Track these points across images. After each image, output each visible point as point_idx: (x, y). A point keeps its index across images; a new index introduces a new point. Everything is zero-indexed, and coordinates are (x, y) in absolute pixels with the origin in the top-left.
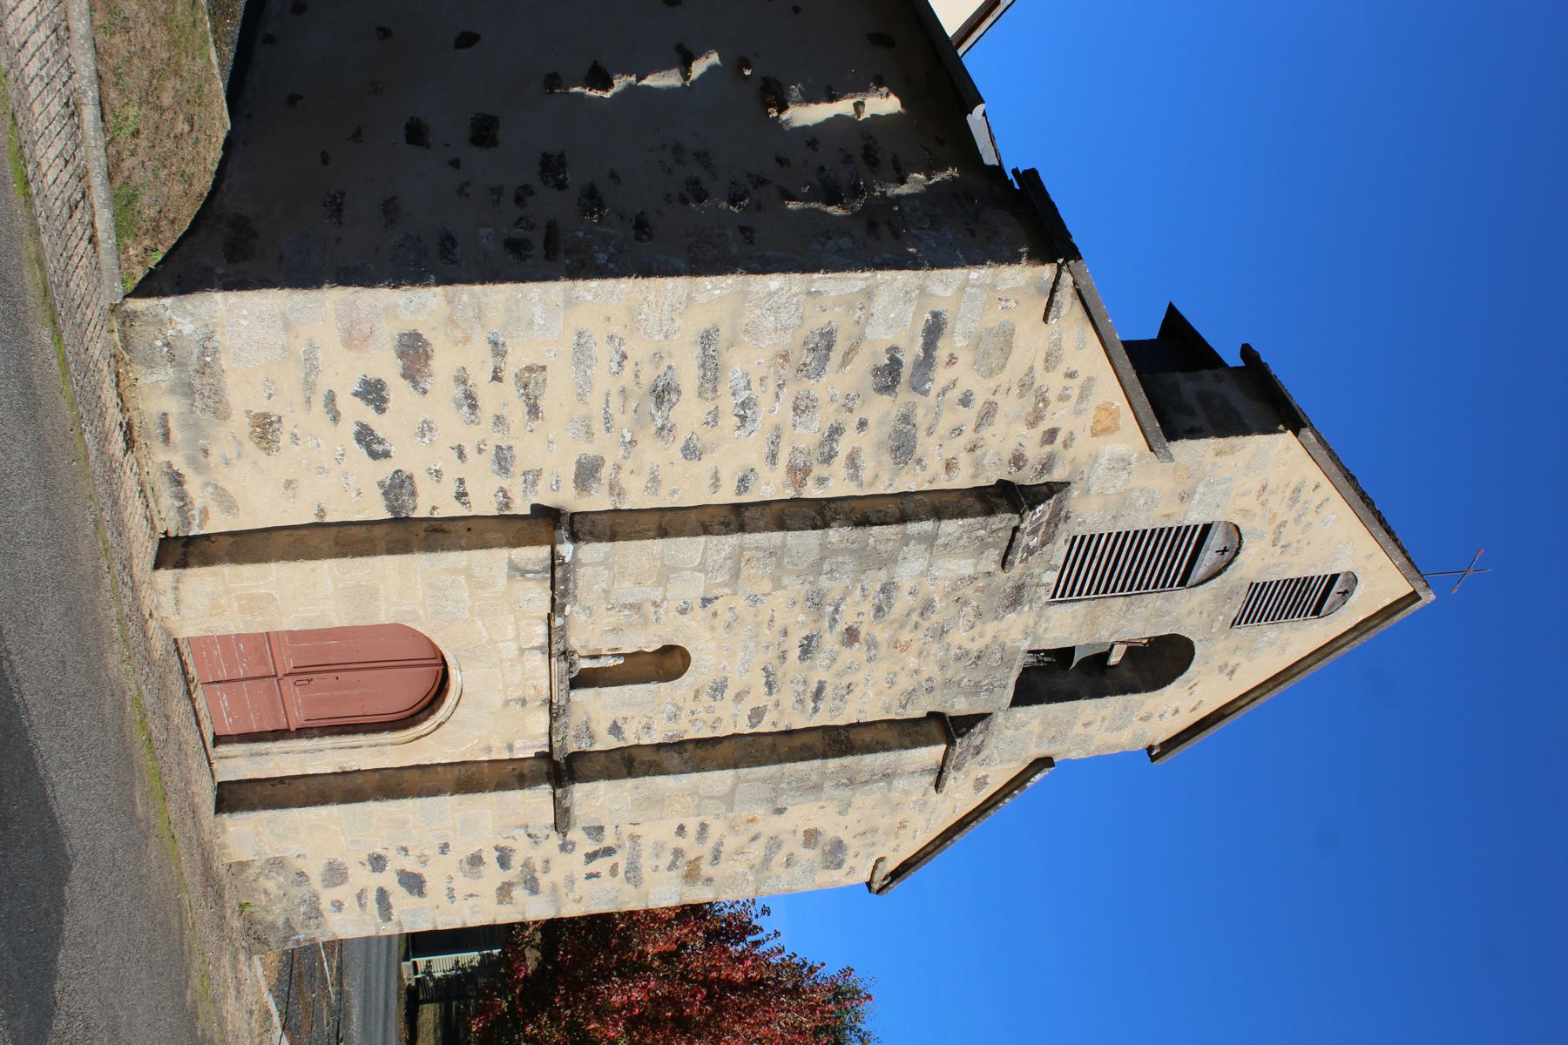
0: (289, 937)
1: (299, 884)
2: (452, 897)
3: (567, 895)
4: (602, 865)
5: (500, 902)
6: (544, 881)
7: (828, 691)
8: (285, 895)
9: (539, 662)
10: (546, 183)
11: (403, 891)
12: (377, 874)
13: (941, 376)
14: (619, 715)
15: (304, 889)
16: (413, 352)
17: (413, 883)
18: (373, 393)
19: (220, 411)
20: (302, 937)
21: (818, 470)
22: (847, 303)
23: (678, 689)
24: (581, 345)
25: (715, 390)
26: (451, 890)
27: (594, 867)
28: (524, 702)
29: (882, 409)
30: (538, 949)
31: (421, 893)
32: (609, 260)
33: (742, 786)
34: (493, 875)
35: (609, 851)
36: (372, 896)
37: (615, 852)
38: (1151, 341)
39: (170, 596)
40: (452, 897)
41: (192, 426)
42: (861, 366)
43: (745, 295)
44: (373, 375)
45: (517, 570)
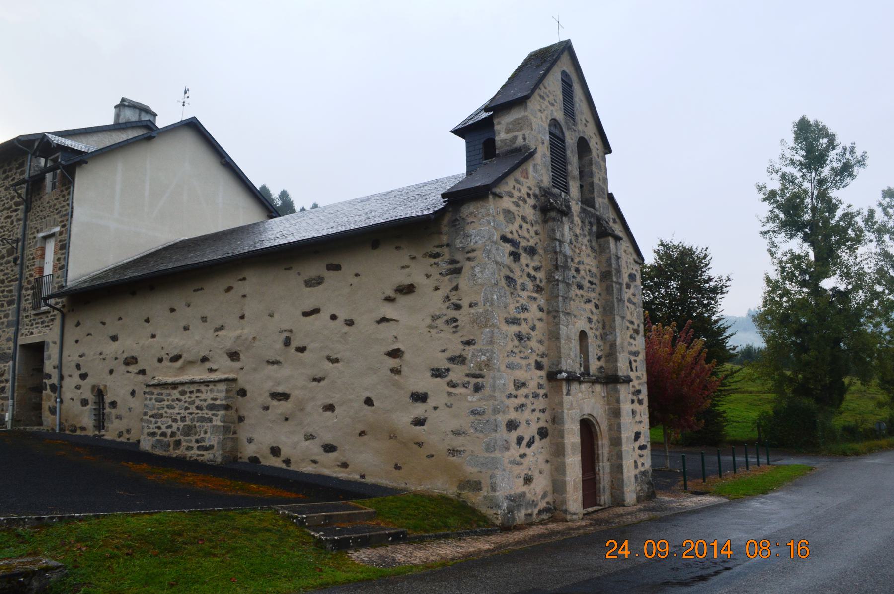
7: (591, 279)
10: (446, 376)
13: (515, 236)
14: (596, 357)
18: (520, 440)
19: (523, 495)
21: (538, 282)
23: (590, 334)
24: (509, 366)
25: (519, 319)
27: (634, 369)
29: (524, 258)
30: (774, 392)
32: (485, 355)
33: (620, 313)
38: (467, 143)
42: (513, 266)
45: (568, 394)
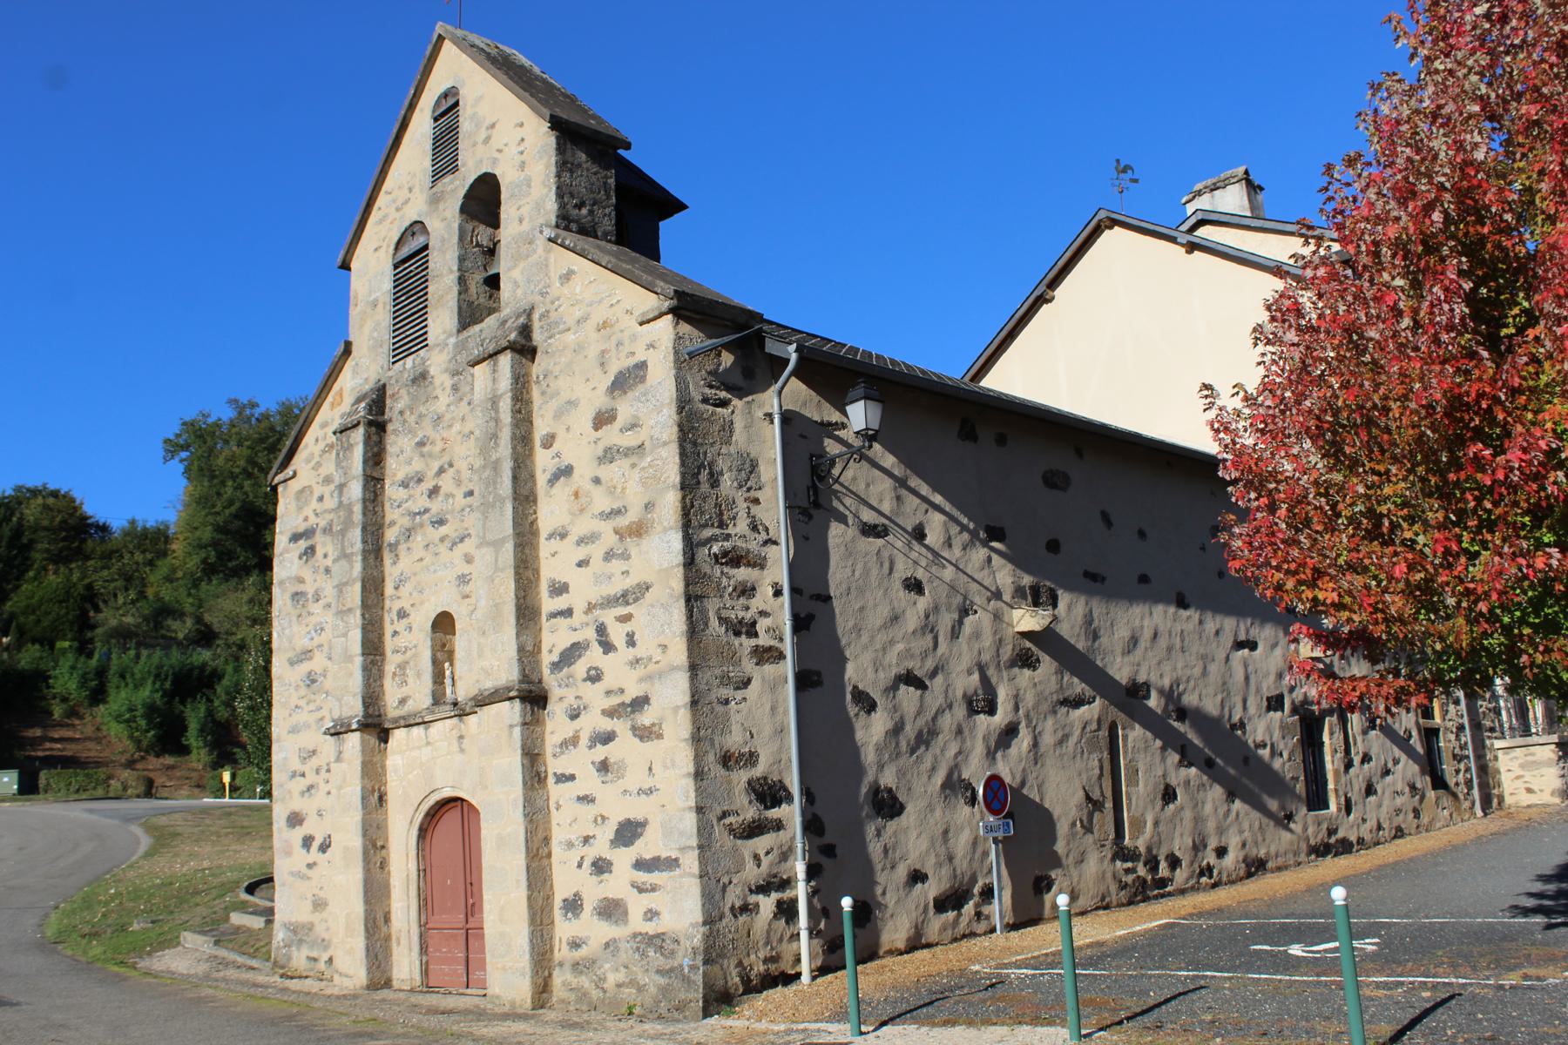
0: (683, 975)
1: (617, 949)
2: (650, 792)
3: (657, 662)
4: (617, 634)
5: (660, 736)
6: (633, 691)
8: (626, 967)
9: (436, 728)
11: (639, 843)
12: (614, 868)
15: (623, 945)
16: (295, 820)
17: (628, 832)
18: (307, 842)
20: (687, 962)
22: (284, 591)
26: (641, 792)
28: (461, 737)
31: (643, 824)
34: (626, 748)
35: (601, 630)
36: (642, 877)
37: (602, 624)
39: (344, 979)
40: (650, 792)
41: (312, 945)
43: (279, 649)
44: (300, 842)
